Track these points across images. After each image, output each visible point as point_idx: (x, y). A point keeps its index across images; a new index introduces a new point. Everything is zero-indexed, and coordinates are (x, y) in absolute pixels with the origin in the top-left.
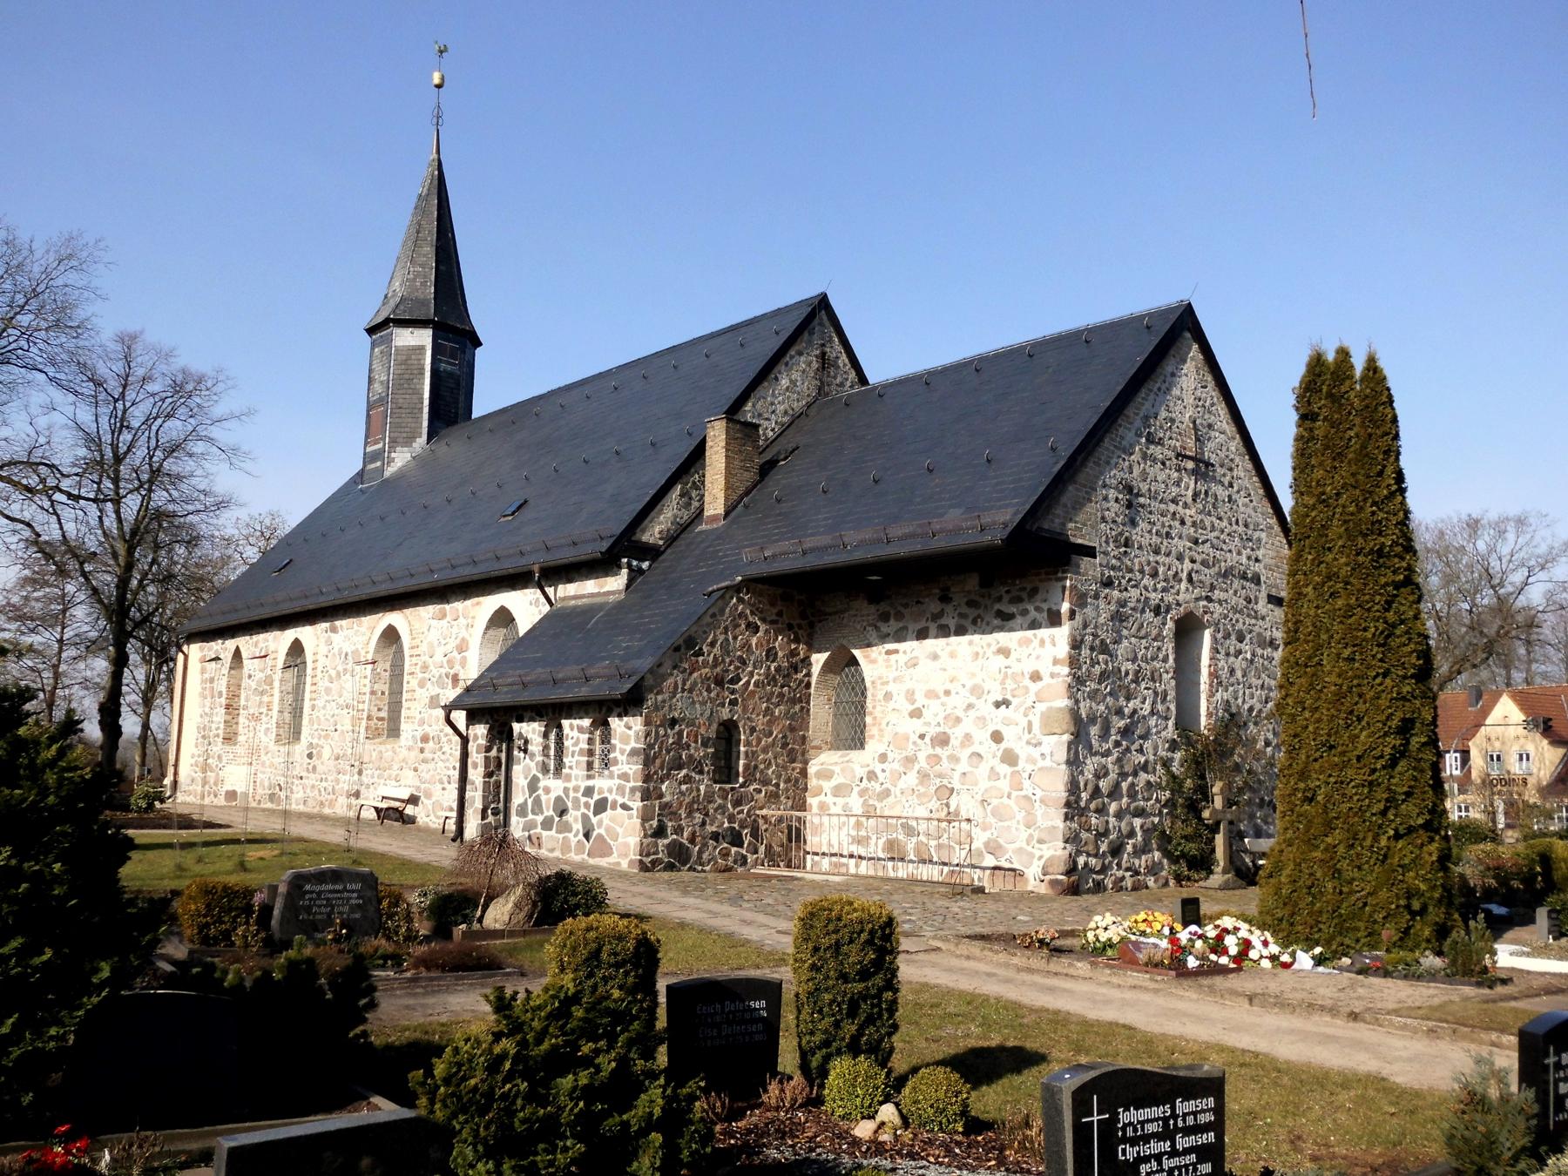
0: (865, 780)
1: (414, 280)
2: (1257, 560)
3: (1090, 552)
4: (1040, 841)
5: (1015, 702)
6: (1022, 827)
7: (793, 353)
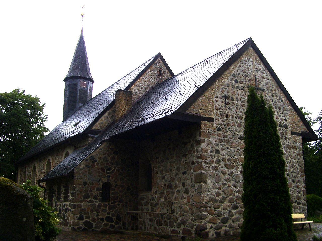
0: (152, 200)
1: (75, 66)
2: (286, 120)
3: (211, 120)
4: (195, 220)
5: (188, 172)
6: (190, 215)
7: (149, 71)
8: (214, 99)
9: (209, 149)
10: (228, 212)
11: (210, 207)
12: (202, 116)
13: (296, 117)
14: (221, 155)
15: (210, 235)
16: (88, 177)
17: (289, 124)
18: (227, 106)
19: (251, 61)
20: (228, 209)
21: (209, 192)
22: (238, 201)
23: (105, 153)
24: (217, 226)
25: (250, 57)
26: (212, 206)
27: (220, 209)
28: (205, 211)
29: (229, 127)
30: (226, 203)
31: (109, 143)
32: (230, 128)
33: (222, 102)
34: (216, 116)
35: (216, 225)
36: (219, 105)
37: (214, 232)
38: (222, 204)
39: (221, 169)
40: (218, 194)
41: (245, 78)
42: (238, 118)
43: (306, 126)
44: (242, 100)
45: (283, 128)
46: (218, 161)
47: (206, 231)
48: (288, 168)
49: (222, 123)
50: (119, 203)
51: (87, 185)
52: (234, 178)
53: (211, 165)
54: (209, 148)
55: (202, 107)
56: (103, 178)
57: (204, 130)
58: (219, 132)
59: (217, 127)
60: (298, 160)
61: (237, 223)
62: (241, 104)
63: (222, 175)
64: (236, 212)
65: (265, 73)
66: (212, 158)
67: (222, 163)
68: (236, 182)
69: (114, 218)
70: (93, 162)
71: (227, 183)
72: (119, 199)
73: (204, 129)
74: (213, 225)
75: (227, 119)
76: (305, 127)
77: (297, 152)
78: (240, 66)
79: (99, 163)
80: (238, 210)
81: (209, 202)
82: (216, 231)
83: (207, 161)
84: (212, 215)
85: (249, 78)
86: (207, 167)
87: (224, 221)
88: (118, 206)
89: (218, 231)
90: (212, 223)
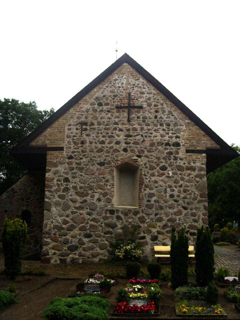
3: (62, 149)
8: (66, 128)
9: (55, 178)
10: (77, 240)
11: (55, 234)
12: (48, 146)
13: (198, 131)
14: (71, 183)
15: (52, 261)
16: (8, 206)
17: (183, 141)
18: (83, 132)
19: (125, 78)
20: (78, 237)
21: (54, 219)
22: (91, 230)
23: (25, 185)
24: (61, 253)
25: (123, 74)
26: (57, 233)
27: (67, 237)
28: (48, 237)
29: (84, 154)
30: (76, 231)
31: (29, 175)
32: (85, 155)
33: (77, 129)
34: (67, 144)
35: (61, 252)
36: (72, 133)
37: (58, 259)
38: (71, 232)
39: (70, 197)
40: (65, 222)
41: (114, 99)
42: (98, 143)
43: (214, 141)
44: (106, 123)
45: (172, 147)
46: (66, 190)
47: (47, 256)
48: (177, 193)
49: (75, 150)
50: (37, 228)
51: (7, 213)
52: (88, 206)
53: (57, 194)
54: (56, 177)
55: (50, 138)
56: (22, 206)
57: (51, 160)
58: (70, 160)
59: (67, 155)
60: (196, 183)
61: (89, 252)
62: (104, 127)
63: (71, 203)
64: (89, 241)
65: (147, 88)
66: (59, 187)
67: (72, 191)
68: (90, 209)
69: (32, 241)
70: (13, 193)
71: (77, 211)
72: (37, 225)
73: (50, 159)
74: (57, 252)
75: (82, 146)
76: (213, 142)
77: (194, 174)
78: (107, 87)
79: (19, 194)
80: (92, 238)
81: (54, 229)
82: (60, 257)
83: (52, 190)
84: (56, 242)
85: (119, 97)
86: (51, 195)
87: (73, 249)
88: (36, 231)
89: (63, 258)
90: (56, 250)
